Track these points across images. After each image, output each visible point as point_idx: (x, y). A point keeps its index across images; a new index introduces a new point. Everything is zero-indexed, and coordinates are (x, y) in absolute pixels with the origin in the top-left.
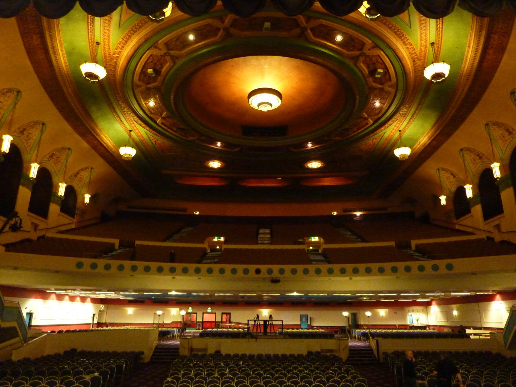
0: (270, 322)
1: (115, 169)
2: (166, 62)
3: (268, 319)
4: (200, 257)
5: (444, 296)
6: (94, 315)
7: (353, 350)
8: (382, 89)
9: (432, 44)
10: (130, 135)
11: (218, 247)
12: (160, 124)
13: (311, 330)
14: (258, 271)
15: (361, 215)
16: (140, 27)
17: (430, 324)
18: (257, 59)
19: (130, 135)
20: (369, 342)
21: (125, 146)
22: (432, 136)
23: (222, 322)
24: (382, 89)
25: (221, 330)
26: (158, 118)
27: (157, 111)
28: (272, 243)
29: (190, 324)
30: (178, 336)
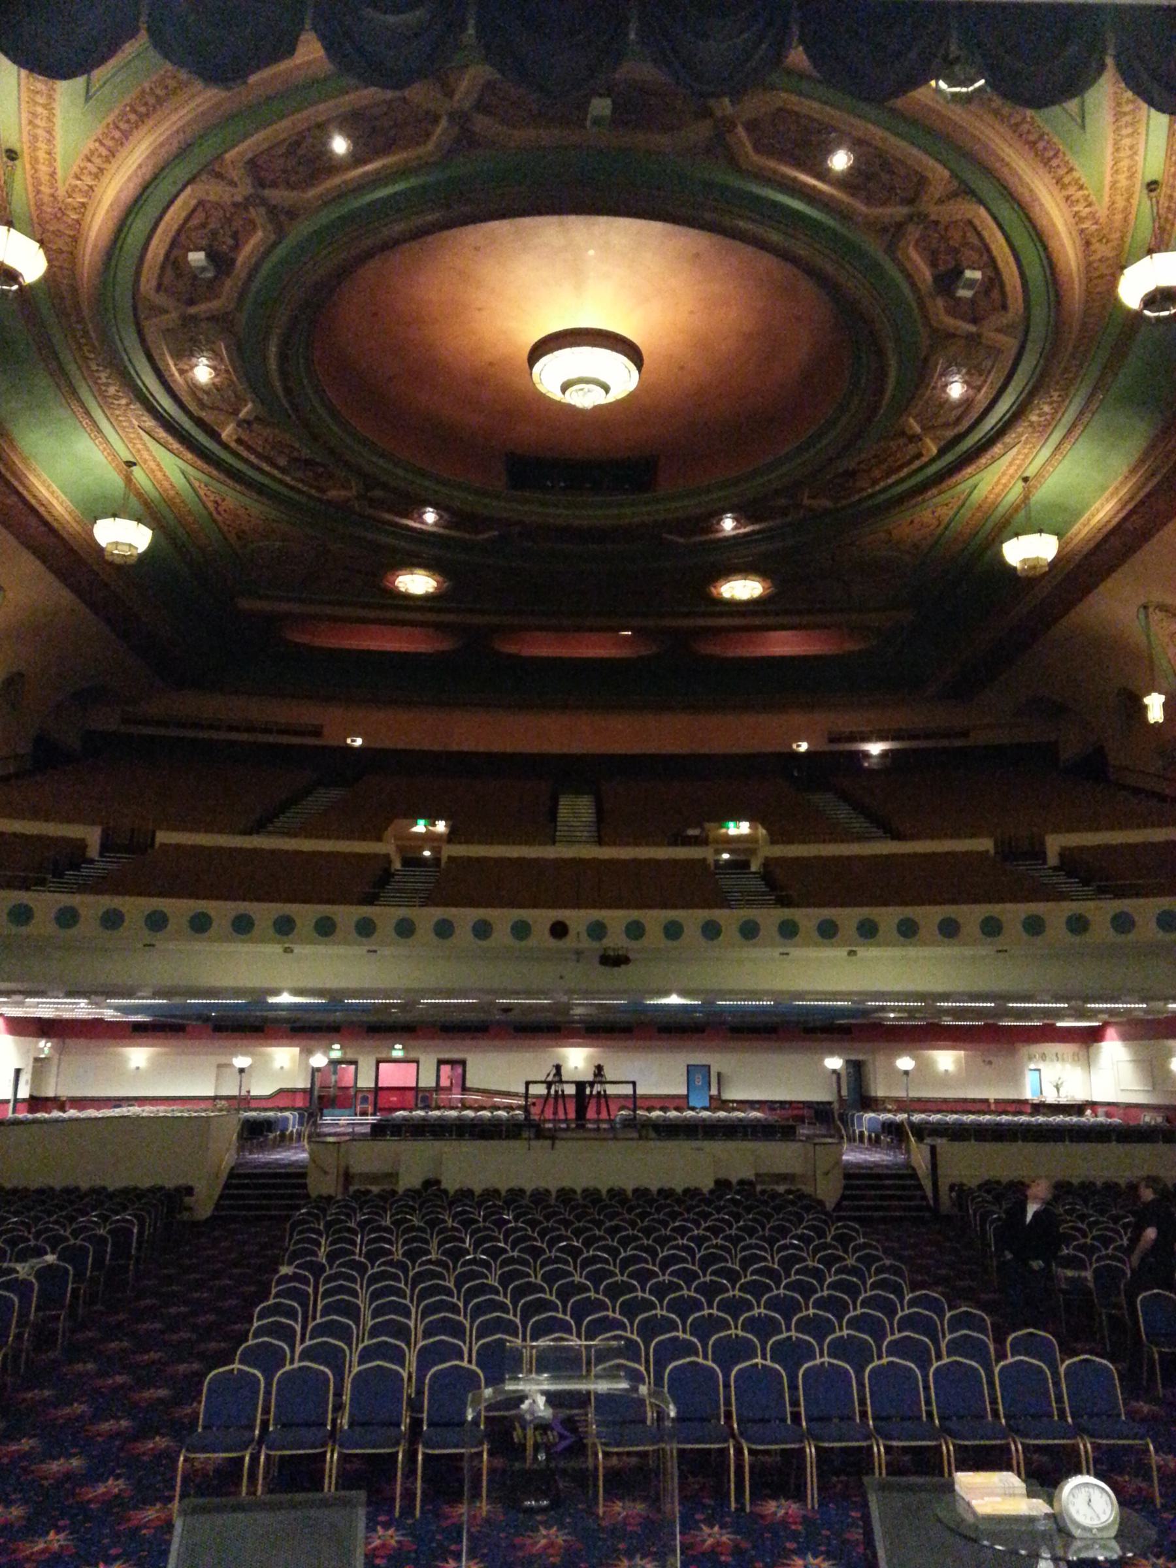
0: (597, 1088)
1: (76, 589)
2: (252, 226)
3: (590, 1078)
4: (372, 884)
5: (1145, 1011)
6: (18, 1072)
7: (855, 1177)
8: (973, 340)
9: (1152, 186)
10: (128, 480)
11: (427, 853)
12: (233, 445)
13: (722, 1114)
14: (559, 930)
15: (885, 754)
16: (160, 101)
17: (1097, 1098)
18: (561, 224)
19: (128, 480)
20: (908, 1151)
21: (115, 516)
22: (1132, 499)
23: (438, 1088)
24: (973, 340)
25: (437, 1113)
26: (224, 425)
27: (218, 398)
28: (600, 842)
29: (336, 1097)
30: (299, 1134)
